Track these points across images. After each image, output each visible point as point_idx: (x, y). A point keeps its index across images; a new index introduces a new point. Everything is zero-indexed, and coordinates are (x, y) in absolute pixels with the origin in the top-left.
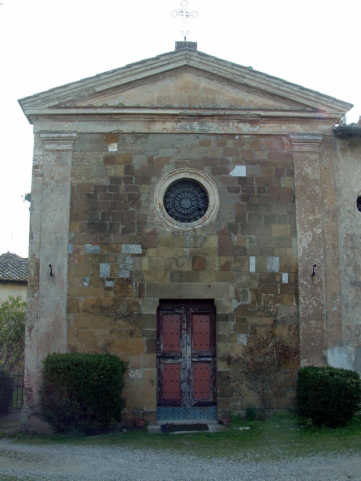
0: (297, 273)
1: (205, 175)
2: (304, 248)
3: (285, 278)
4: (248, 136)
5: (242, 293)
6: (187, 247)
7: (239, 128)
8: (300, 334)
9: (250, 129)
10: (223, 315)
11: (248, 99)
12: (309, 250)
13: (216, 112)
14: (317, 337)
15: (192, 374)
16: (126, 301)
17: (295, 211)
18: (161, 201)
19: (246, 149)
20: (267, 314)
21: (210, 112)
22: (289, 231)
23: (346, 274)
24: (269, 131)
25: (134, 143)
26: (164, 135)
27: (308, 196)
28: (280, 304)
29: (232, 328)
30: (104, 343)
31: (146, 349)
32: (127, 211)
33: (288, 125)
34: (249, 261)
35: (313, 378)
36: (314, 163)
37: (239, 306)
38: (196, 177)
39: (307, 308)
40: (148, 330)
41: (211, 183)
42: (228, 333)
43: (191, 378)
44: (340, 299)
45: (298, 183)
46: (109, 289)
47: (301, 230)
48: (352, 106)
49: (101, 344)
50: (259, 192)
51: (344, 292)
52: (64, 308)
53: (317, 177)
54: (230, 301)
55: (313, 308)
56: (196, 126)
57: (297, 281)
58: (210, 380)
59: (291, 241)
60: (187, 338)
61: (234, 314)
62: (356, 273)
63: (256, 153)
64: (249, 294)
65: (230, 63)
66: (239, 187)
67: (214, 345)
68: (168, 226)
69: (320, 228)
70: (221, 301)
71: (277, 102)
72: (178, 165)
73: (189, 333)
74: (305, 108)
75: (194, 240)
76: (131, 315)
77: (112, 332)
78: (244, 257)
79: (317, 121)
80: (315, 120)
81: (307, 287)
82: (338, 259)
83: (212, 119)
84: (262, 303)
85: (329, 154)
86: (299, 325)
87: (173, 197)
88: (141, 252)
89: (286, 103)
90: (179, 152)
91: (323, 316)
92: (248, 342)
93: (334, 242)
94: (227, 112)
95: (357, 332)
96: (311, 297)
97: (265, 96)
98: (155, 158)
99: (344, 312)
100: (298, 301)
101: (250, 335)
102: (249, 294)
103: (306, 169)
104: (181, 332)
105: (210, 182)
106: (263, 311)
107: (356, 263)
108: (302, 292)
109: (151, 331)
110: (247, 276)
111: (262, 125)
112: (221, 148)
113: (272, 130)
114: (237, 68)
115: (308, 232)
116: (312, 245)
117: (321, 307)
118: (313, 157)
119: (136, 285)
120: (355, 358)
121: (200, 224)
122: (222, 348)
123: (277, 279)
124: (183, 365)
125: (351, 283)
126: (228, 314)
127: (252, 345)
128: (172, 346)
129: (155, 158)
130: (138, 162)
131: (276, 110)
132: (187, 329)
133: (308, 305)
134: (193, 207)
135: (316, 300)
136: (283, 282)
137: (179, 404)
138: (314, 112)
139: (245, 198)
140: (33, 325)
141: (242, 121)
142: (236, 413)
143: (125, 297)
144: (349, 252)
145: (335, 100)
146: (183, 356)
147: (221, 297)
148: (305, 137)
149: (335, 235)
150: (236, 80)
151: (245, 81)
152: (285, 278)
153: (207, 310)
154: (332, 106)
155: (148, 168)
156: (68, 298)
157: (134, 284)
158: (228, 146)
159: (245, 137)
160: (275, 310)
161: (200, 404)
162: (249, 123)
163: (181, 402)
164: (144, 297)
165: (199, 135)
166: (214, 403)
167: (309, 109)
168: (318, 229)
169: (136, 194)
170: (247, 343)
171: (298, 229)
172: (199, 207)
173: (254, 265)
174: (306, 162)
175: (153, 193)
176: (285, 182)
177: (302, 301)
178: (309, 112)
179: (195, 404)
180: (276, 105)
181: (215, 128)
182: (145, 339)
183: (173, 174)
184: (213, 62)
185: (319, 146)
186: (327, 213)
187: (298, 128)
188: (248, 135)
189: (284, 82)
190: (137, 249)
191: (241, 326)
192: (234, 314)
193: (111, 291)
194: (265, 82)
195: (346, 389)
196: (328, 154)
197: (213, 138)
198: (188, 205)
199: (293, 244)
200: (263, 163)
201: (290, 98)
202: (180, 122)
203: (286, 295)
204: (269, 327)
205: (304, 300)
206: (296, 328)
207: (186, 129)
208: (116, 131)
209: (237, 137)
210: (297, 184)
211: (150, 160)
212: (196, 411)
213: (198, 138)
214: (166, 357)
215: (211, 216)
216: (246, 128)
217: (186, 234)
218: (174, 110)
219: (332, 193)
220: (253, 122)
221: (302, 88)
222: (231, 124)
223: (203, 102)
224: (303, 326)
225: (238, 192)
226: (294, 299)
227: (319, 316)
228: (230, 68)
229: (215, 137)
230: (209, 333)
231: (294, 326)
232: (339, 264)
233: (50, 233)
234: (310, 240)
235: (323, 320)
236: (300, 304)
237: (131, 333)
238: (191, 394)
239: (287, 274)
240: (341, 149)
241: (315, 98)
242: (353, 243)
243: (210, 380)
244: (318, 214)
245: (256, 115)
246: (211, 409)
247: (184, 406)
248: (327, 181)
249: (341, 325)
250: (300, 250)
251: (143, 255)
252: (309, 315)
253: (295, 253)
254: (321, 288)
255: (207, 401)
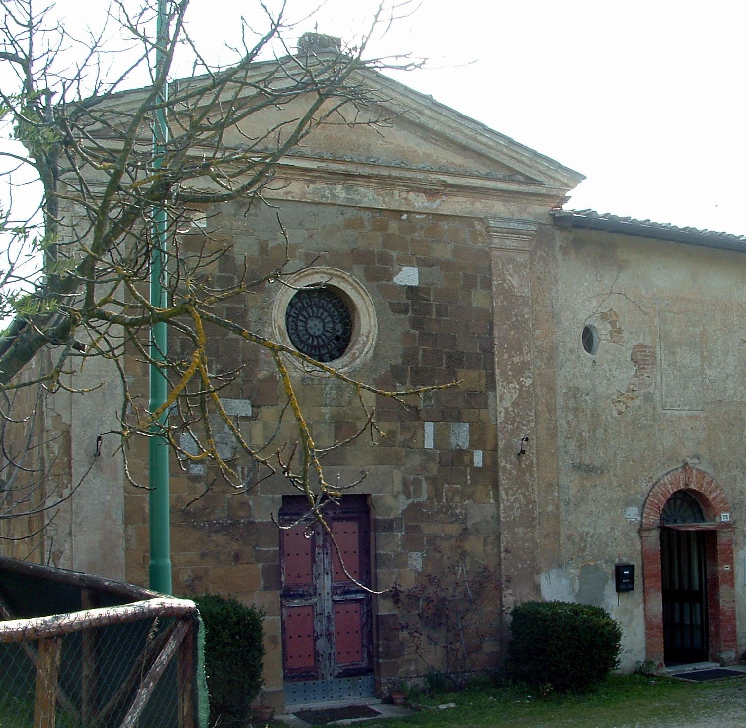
0: (495, 449)
1: (354, 280)
2: (506, 409)
3: (478, 458)
4: (422, 216)
5: (413, 483)
6: (326, 405)
7: (409, 201)
8: (502, 549)
9: (426, 204)
10: (385, 521)
11: (423, 150)
12: (514, 412)
13: (375, 172)
14: (526, 553)
15: (333, 623)
16: (226, 500)
17: (493, 348)
18: (281, 321)
19: (418, 239)
20: (452, 518)
21: (366, 171)
22: (483, 381)
23: (567, 452)
24: (455, 210)
25: (235, 215)
26: (286, 203)
27: (513, 323)
28: (471, 501)
29: (400, 543)
30: (190, 577)
31: (262, 583)
32: (225, 338)
33: (485, 201)
34: (424, 430)
35: (554, 620)
36: (522, 268)
37: (409, 506)
38: (340, 282)
39: (511, 508)
40: (265, 549)
41: (364, 295)
42: (394, 551)
43: (333, 629)
44: (558, 492)
45: (498, 302)
46: (196, 479)
47: (502, 380)
48: (584, 178)
49: (186, 578)
50: (439, 314)
51: (564, 481)
52: (118, 515)
53: (526, 292)
54: (396, 497)
55: (521, 508)
56: (340, 192)
57: (495, 463)
58: (362, 631)
59: (487, 397)
60: (324, 561)
61: (401, 519)
62: (580, 450)
63: (435, 246)
64: (425, 485)
65: (402, 85)
66: (408, 304)
67: (367, 571)
68: (296, 368)
69: (530, 377)
70: (382, 497)
71: (468, 160)
72: (312, 260)
73: (327, 553)
74: (512, 175)
75: (338, 393)
76: (235, 524)
77: (203, 555)
78: (416, 423)
79: (528, 197)
80: (526, 197)
81: (510, 474)
82: (555, 428)
83: (367, 182)
84: (444, 500)
85: (544, 254)
86: (500, 534)
87: (294, 315)
88: (250, 414)
89: (483, 164)
90: (311, 237)
91: (534, 519)
92: (425, 565)
93: (549, 400)
94: (395, 173)
95: (582, 545)
96: (517, 490)
97: (451, 148)
98: (271, 244)
99: (564, 514)
100: (498, 495)
101: (427, 553)
102: (425, 485)
103: (510, 278)
104: (314, 551)
105: (362, 292)
106: (446, 513)
107: (581, 434)
108: (503, 481)
109: (270, 551)
110: (421, 455)
111: (444, 198)
112: (380, 233)
113: (460, 208)
114: (413, 96)
115: (512, 383)
116: (518, 404)
117: (531, 506)
118: (520, 258)
119: (243, 472)
120: (580, 586)
121: (346, 366)
122: (387, 577)
123: (466, 459)
124: (318, 609)
125: (574, 467)
126: (392, 519)
127: (429, 569)
128: (299, 576)
129: (271, 244)
130: (244, 250)
131: (472, 176)
132: (324, 546)
133: (513, 503)
134: (328, 334)
135: (524, 495)
136: (475, 465)
137: (314, 675)
138: (527, 183)
139: (417, 323)
140: (62, 549)
141: (415, 189)
142: (409, 684)
143: (224, 492)
144: (571, 417)
145: (560, 166)
146: (318, 592)
147: (381, 491)
148: (513, 225)
149: (551, 389)
150: (408, 117)
151: (423, 120)
152: (478, 458)
153: (355, 513)
154: (554, 175)
155: (260, 263)
156: (125, 497)
157: (239, 469)
158: (390, 231)
159: (418, 216)
160: (464, 512)
161: (349, 673)
162: (425, 193)
163: (317, 672)
164: (257, 492)
165: (344, 208)
166: (369, 670)
167: (521, 178)
168: (526, 378)
169: (241, 309)
170: (422, 567)
171: (498, 377)
172: (337, 333)
173: (432, 437)
174: (511, 266)
175: (268, 309)
176: (478, 299)
177: (504, 496)
178: (519, 182)
179: (340, 673)
180: (465, 165)
181: (371, 198)
182: (260, 565)
183: (302, 275)
184: (373, 80)
185: (530, 241)
186: (540, 352)
187: (499, 207)
188: (423, 213)
189: (485, 129)
190: (243, 407)
191: (413, 541)
192: (401, 519)
193: (200, 482)
194: (454, 125)
195: (602, 634)
196: (542, 255)
197: (366, 215)
198: (319, 330)
199: (490, 402)
200: (446, 265)
201: (492, 156)
202: (314, 182)
203: (480, 487)
204: (455, 539)
205: (507, 494)
206: (494, 540)
207: (324, 196)
208: (205, 189)
209: (404, 217)
210: (497, 303)
211: (263, 248)
212: (341, 685)
213: (342, 214)
214: (290, 596)
215: (364, 353)
216: (419, 202)
217: (324, 383)
218: (308, 162)
219: (547, 320)
220: (431, 193)
221: (511, 142)
222: (396, 193)
223: (351, 150)
224: (505, 537)
225: (406, 311)
226: (491, 492)
227: (529, 520)
228: (401, 94)
229: (370, 214)
230: (357, 551)
231: (492, 537)
232: (556, 436)
233: (89, 375)
234: (515, 396)
235: (534, 527)
236: (501, 502)
237: (237, 557)
238: (332, 656)
239: (481, 452)
240: (561, 247)
241: (531, 160)
242: (577, 403)
243: (362, 631)
244: (527, 353)
245: (439, 181)
246: (364, 680)
247: (323, 679)
248: (540, 300)
249: (559, 534)
250: (500, 413)
251: (254, 417)
252: (514, 519)
253: (493, 418)
254: (532, 475)
255: (359, 666)
